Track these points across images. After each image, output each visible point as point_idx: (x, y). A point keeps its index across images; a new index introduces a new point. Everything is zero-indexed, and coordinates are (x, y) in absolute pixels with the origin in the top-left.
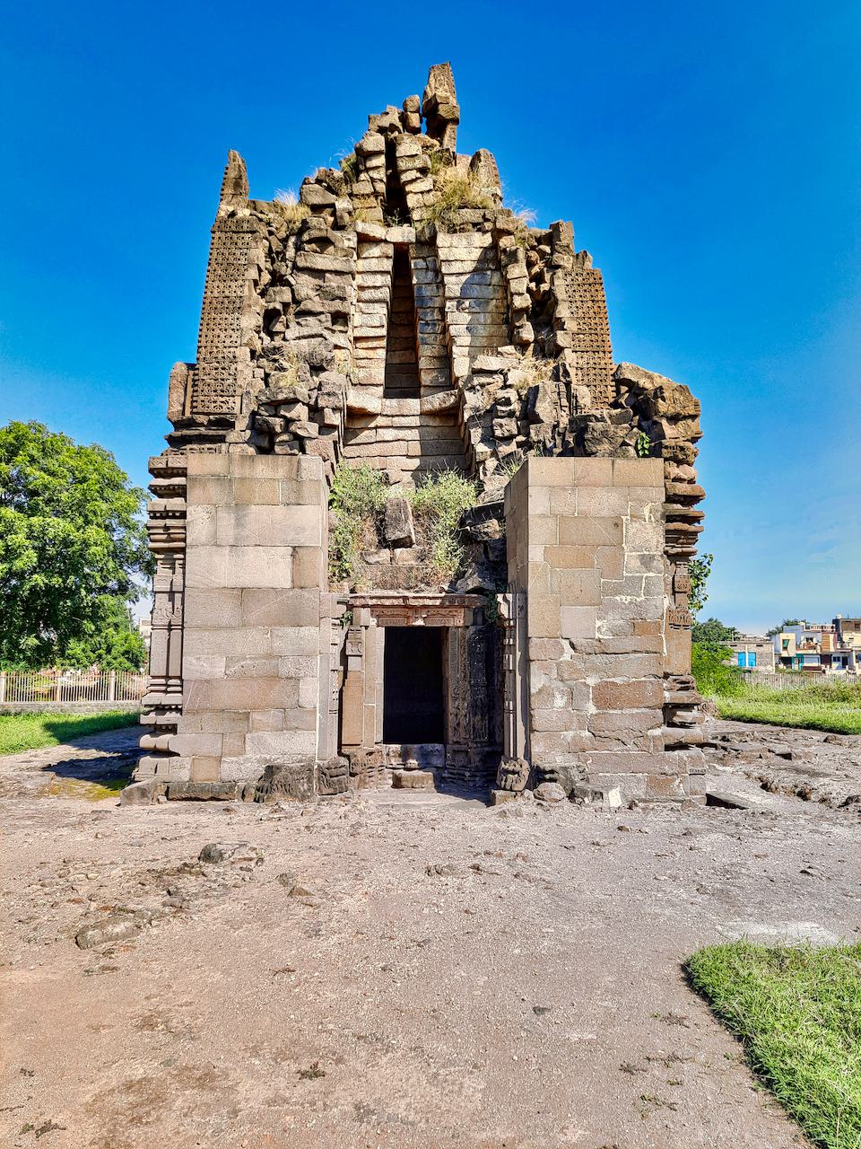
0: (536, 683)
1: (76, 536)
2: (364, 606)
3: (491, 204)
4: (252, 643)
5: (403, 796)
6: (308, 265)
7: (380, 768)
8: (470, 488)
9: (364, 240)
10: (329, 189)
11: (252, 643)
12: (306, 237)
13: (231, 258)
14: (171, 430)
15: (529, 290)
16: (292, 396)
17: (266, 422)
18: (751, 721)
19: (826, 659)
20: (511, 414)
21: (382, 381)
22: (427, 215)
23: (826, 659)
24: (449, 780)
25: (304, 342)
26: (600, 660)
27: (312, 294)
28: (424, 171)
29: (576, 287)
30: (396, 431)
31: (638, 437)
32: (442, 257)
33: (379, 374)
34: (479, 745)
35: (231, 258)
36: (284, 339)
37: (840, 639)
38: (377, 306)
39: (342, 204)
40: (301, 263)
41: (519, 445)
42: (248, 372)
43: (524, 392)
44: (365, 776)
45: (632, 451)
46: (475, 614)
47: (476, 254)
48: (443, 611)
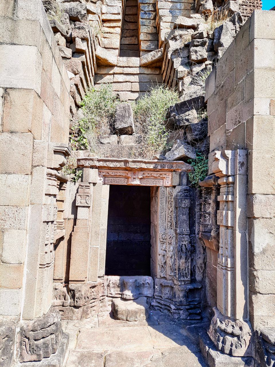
2: (92, 167)
5: (120, 328)
7: (102, 298)
24: (156, 308)
30: (125, 76)
33: (117, 43)
34: (183, 283)
44: (87, 308)
46: (181, 176)
48: (155, 174)
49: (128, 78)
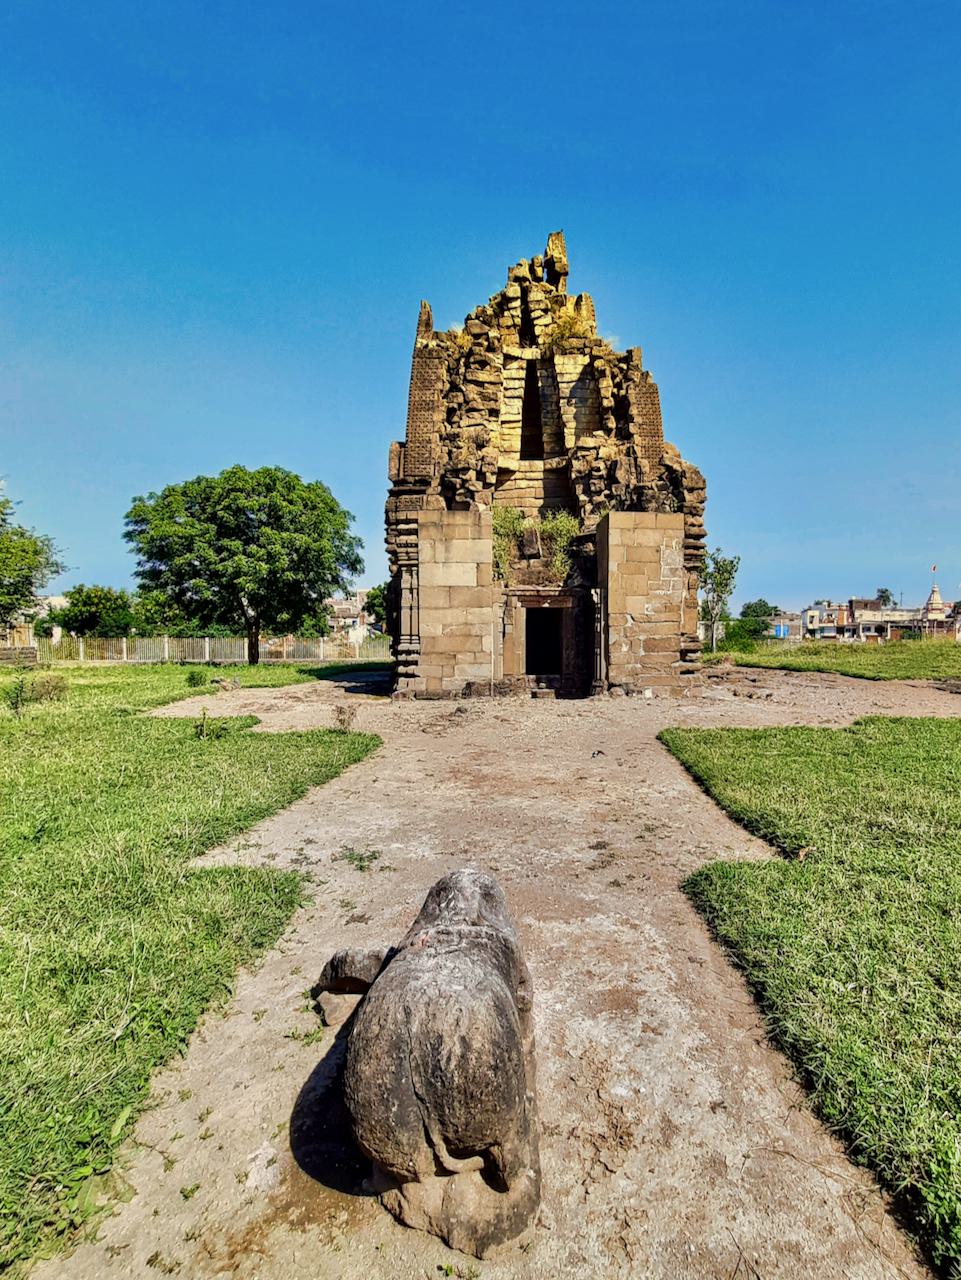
0: (612, 640)
1: (314, 546)
3: (589, 334)
4: (456, 616)
6: (474, 378)
8: (575, 522)
9: (509, 358)
10: (484, 322)
11: (456, 616)
12: (472, 360)
13: (426, 375)
14: (391, 486)
15: (613, 395)
16: (466, 465)
17: (451, 482)
18: (752, 666)
19: (841, 630)
20: (601, 477)
21: (542, 496)
22: (549, 340)
23: (841, 630)
25: (472, 428)
26: (647, 626)
27: (476, 397)
28: (546, 311)
29: (641, 395)
30: (527, 482)
31: (670, 501)
32: (558, 371)
33: (517, 445)
35: (426, 375)
36: (459, 427)
37: (852, 615)
38: (516, 400)
39: (493, 333)
40: (469, 377)
41: (606, 496)
42: (438, 449)
43: (609, 463)
45: (668, 508)
47: (580, 369)
48: (559, 598)
49: (531, 483)
